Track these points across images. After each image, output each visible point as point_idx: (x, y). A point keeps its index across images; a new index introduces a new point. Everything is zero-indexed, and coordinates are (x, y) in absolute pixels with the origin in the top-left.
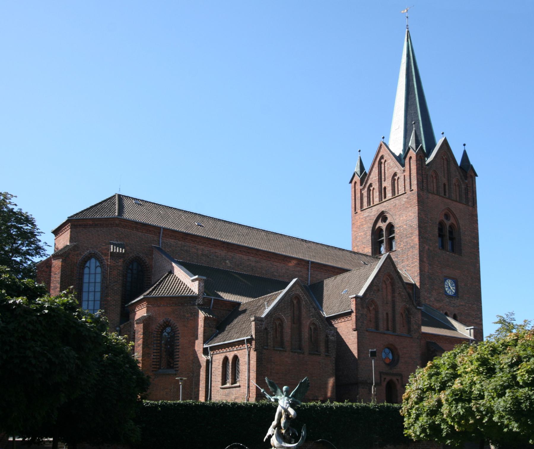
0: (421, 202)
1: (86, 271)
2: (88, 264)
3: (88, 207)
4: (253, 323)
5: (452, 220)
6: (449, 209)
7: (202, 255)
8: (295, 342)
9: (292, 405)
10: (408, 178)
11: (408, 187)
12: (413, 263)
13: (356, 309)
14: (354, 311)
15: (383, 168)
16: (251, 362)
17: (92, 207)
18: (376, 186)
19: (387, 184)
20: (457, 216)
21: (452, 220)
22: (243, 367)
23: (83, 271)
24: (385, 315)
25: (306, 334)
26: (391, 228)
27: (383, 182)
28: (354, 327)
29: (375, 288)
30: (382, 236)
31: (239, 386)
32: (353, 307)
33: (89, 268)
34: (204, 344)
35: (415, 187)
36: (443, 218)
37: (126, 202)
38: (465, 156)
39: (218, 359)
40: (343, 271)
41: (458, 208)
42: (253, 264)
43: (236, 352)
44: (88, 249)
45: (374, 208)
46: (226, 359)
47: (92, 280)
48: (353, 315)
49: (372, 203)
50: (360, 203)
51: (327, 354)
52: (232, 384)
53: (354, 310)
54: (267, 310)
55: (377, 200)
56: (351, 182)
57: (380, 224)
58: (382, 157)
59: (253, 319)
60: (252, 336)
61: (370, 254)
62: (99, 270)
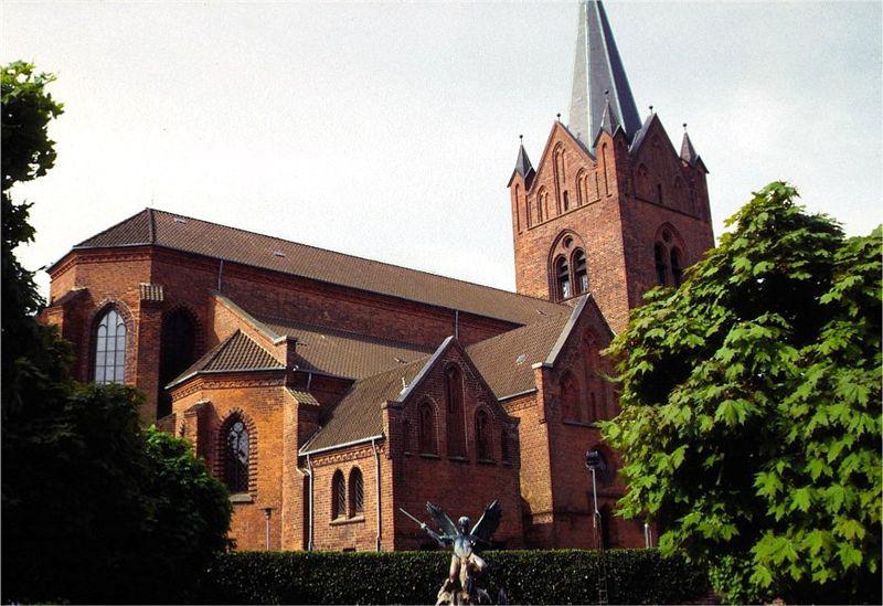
0: (625, 214)
1: (102, 332)
2: (104, 322)
3: (105, 229)
4: (385, 412)
5: (675, 242)
6: (668, 224)
7: (286, 302)
8: (449, 439)
9: (476, 550)
10: (603, 181)
11: (603, 192)
12: (618, 311)
13: (544, 387)
14: (541, 391)
15: (560, 163)
16: (384, 478)
17: (110, 230)
18: (551, 190)
19: (568, 186)
20: (683, 237)
21: (675, 242)
22: (370, 488)
23: (97, 332)
24: (590, 396)
25: (469, 431)
26: (578, 253)
27: (561, 184)
28: (542, 417)
29: (572, 351)
30: (567, 269)
31: (364, 521)
32: (539, 384)
33: (107, 327)
34: (299, 446)
35: (614, 192)
36: (661, 238)
37: (157, 218)
38: (687, 140)
39: (324, 477)
40: (522, 326)
41: (682, 224)
42: (367, 317)
43: (356, 463)
44: (104, 297)
45: (550, 226)
46: (338, 475)
47: (111, 347)
48: (540, 395)
49: (544, 217)
50: (524, 219)
51: (505, 462)
52: (351, 517)
53: (540, 387)
54: (405, 391)
55: (553, 213)
56: (509, 185)
57: (560, 250)
58: (559, 145)
59: (385, 404)
60: (383, 434)
61: (547, 299)
62: (122, 330)
